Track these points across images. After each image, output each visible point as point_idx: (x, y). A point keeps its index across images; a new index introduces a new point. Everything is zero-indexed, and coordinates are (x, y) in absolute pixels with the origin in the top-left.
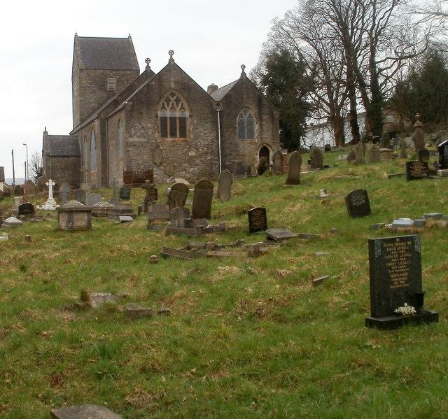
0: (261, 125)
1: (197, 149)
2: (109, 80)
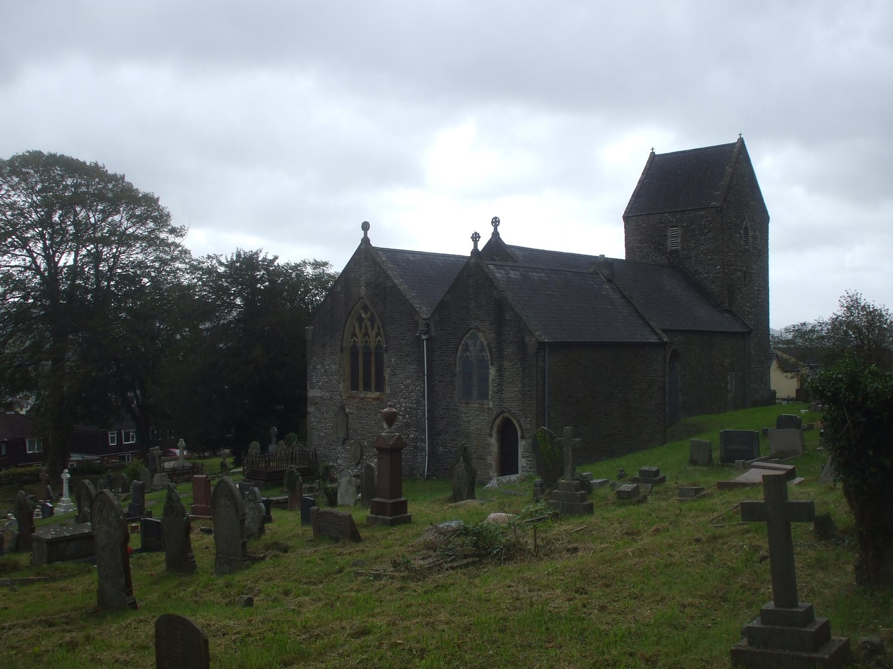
0: (500, 371)
2: (670, 232)
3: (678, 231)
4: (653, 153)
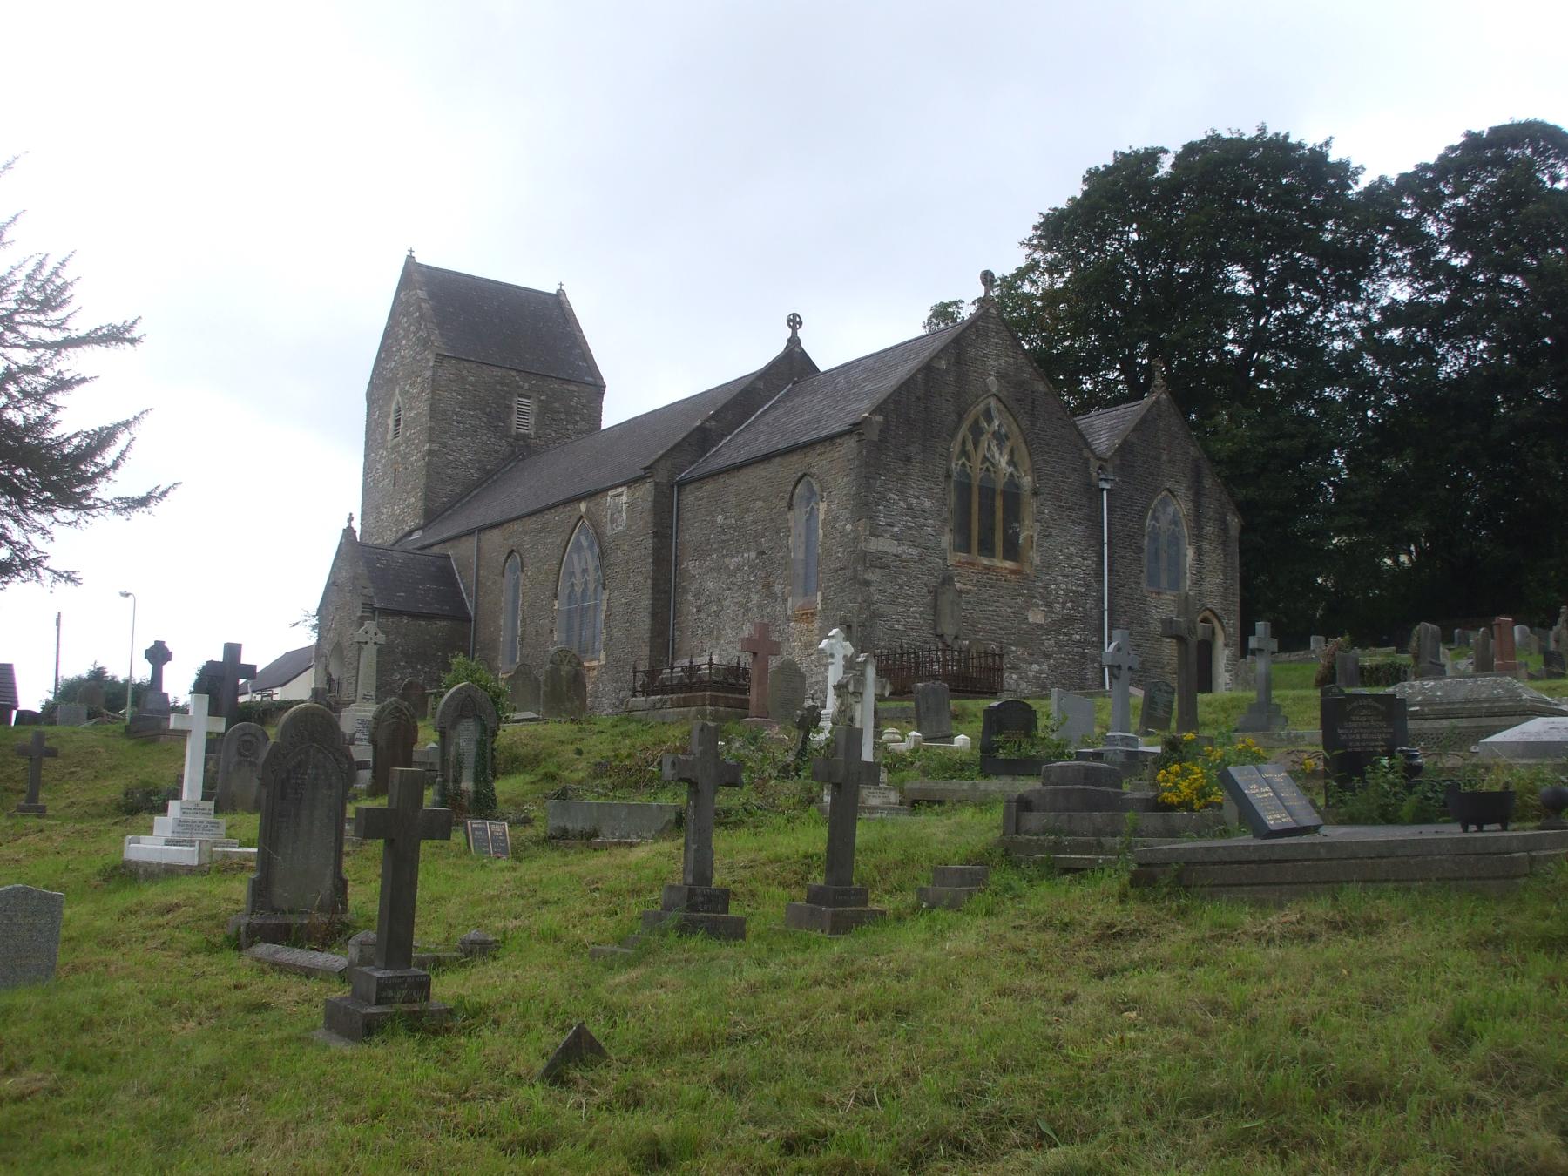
0: (1199, 552)
1: (1049, 605)
3: (532, 405)
4: (410, 261)
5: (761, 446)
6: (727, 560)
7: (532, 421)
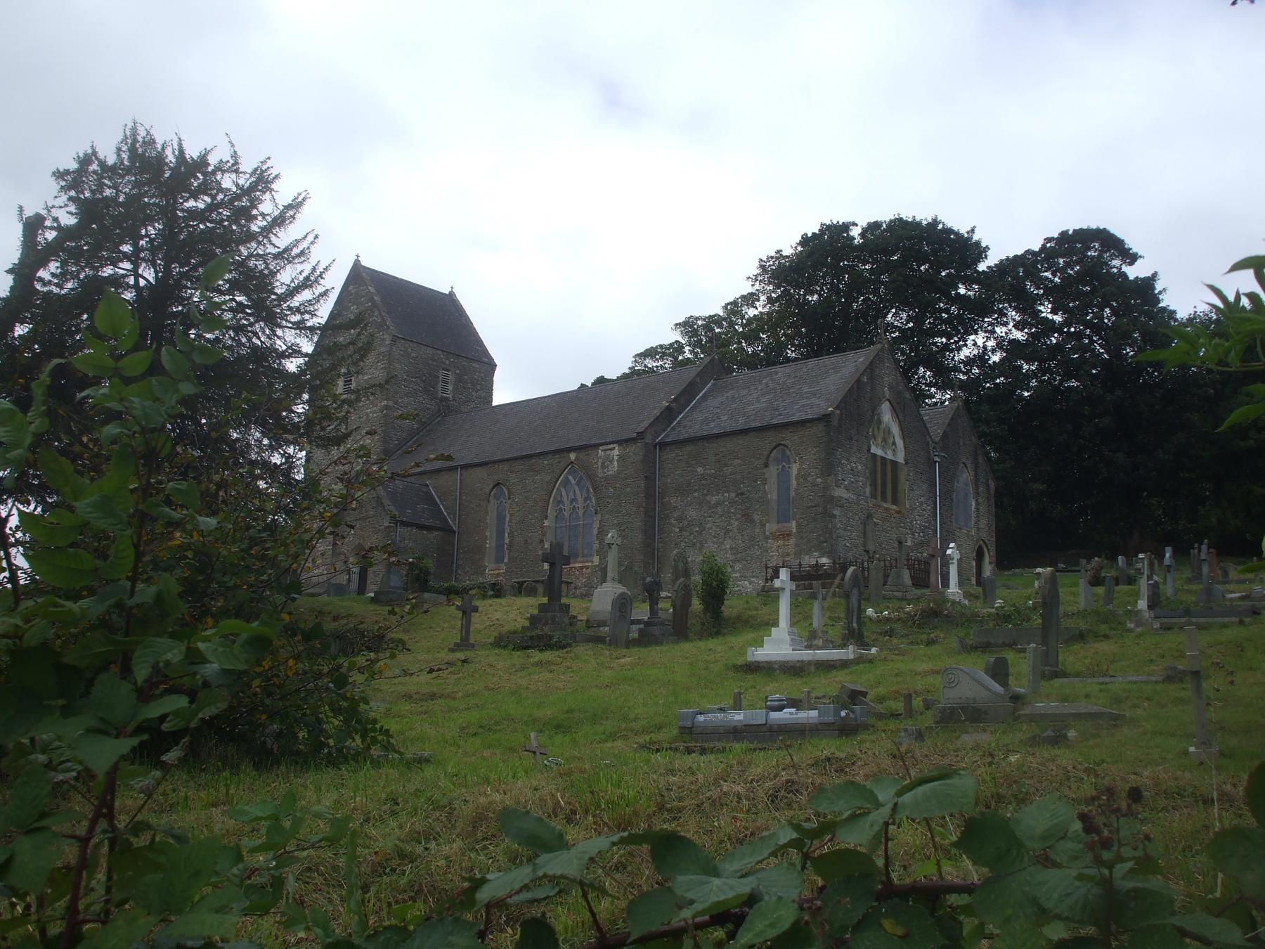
0: (977, 504)
4: (357, 264)
5: (725, 423)
6: (708, 498)
7: (450, 388)
